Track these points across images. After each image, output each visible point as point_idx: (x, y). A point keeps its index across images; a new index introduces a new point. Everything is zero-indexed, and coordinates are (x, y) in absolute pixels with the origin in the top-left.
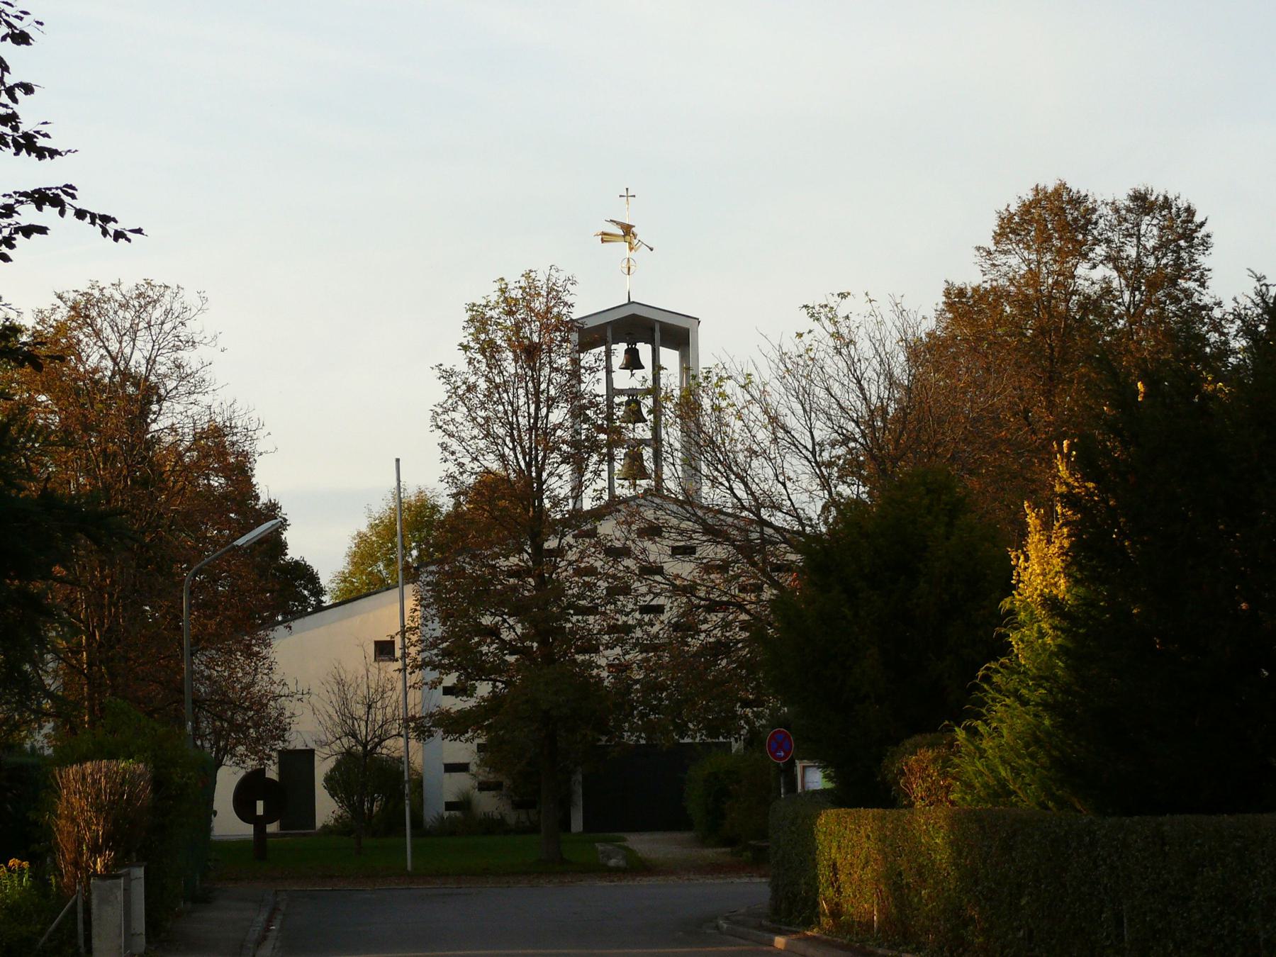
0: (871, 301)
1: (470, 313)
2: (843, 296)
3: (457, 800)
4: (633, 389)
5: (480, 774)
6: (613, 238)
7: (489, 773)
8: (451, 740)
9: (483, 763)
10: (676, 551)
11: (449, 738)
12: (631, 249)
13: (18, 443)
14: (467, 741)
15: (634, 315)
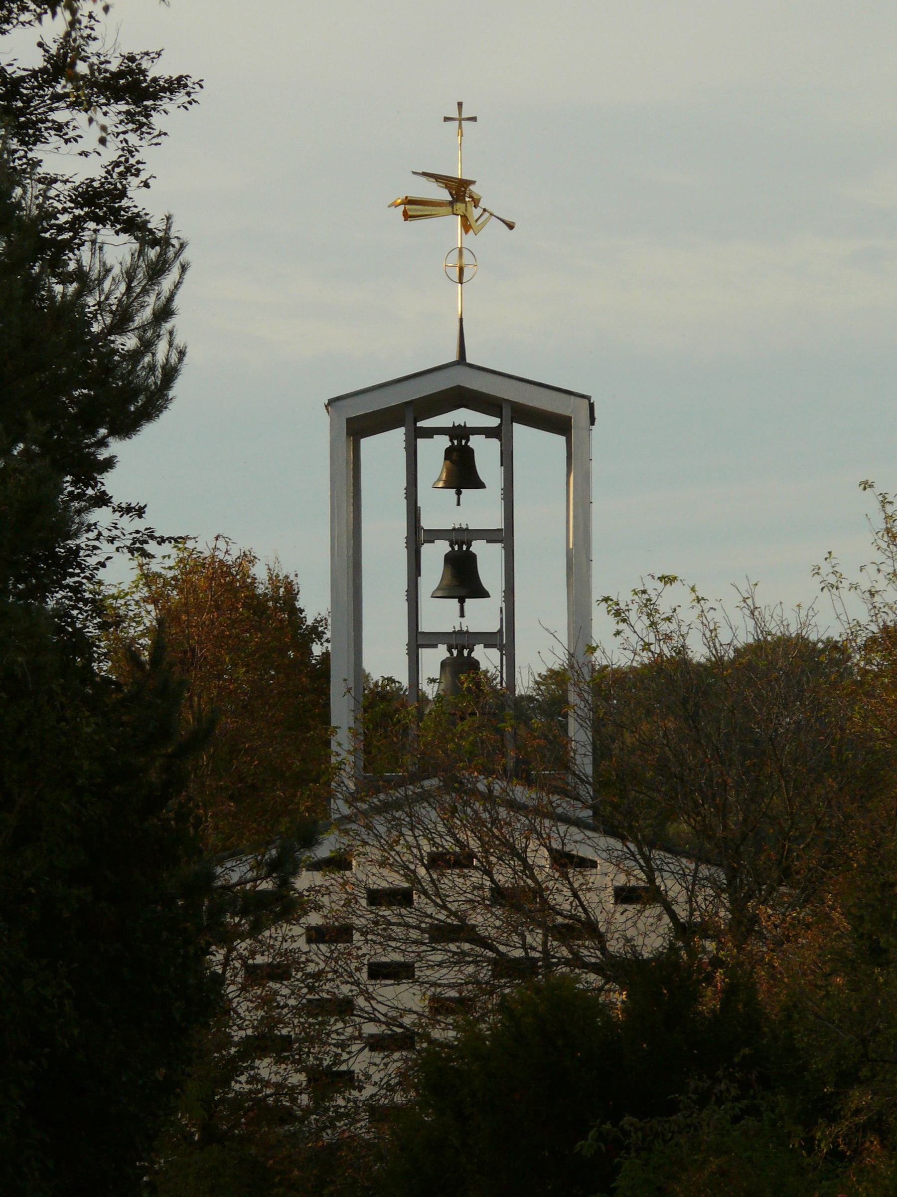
0: (699, 601)
2: (668, 580)
4: (460, 530)
12: (467, 226)
13: (537, 977)
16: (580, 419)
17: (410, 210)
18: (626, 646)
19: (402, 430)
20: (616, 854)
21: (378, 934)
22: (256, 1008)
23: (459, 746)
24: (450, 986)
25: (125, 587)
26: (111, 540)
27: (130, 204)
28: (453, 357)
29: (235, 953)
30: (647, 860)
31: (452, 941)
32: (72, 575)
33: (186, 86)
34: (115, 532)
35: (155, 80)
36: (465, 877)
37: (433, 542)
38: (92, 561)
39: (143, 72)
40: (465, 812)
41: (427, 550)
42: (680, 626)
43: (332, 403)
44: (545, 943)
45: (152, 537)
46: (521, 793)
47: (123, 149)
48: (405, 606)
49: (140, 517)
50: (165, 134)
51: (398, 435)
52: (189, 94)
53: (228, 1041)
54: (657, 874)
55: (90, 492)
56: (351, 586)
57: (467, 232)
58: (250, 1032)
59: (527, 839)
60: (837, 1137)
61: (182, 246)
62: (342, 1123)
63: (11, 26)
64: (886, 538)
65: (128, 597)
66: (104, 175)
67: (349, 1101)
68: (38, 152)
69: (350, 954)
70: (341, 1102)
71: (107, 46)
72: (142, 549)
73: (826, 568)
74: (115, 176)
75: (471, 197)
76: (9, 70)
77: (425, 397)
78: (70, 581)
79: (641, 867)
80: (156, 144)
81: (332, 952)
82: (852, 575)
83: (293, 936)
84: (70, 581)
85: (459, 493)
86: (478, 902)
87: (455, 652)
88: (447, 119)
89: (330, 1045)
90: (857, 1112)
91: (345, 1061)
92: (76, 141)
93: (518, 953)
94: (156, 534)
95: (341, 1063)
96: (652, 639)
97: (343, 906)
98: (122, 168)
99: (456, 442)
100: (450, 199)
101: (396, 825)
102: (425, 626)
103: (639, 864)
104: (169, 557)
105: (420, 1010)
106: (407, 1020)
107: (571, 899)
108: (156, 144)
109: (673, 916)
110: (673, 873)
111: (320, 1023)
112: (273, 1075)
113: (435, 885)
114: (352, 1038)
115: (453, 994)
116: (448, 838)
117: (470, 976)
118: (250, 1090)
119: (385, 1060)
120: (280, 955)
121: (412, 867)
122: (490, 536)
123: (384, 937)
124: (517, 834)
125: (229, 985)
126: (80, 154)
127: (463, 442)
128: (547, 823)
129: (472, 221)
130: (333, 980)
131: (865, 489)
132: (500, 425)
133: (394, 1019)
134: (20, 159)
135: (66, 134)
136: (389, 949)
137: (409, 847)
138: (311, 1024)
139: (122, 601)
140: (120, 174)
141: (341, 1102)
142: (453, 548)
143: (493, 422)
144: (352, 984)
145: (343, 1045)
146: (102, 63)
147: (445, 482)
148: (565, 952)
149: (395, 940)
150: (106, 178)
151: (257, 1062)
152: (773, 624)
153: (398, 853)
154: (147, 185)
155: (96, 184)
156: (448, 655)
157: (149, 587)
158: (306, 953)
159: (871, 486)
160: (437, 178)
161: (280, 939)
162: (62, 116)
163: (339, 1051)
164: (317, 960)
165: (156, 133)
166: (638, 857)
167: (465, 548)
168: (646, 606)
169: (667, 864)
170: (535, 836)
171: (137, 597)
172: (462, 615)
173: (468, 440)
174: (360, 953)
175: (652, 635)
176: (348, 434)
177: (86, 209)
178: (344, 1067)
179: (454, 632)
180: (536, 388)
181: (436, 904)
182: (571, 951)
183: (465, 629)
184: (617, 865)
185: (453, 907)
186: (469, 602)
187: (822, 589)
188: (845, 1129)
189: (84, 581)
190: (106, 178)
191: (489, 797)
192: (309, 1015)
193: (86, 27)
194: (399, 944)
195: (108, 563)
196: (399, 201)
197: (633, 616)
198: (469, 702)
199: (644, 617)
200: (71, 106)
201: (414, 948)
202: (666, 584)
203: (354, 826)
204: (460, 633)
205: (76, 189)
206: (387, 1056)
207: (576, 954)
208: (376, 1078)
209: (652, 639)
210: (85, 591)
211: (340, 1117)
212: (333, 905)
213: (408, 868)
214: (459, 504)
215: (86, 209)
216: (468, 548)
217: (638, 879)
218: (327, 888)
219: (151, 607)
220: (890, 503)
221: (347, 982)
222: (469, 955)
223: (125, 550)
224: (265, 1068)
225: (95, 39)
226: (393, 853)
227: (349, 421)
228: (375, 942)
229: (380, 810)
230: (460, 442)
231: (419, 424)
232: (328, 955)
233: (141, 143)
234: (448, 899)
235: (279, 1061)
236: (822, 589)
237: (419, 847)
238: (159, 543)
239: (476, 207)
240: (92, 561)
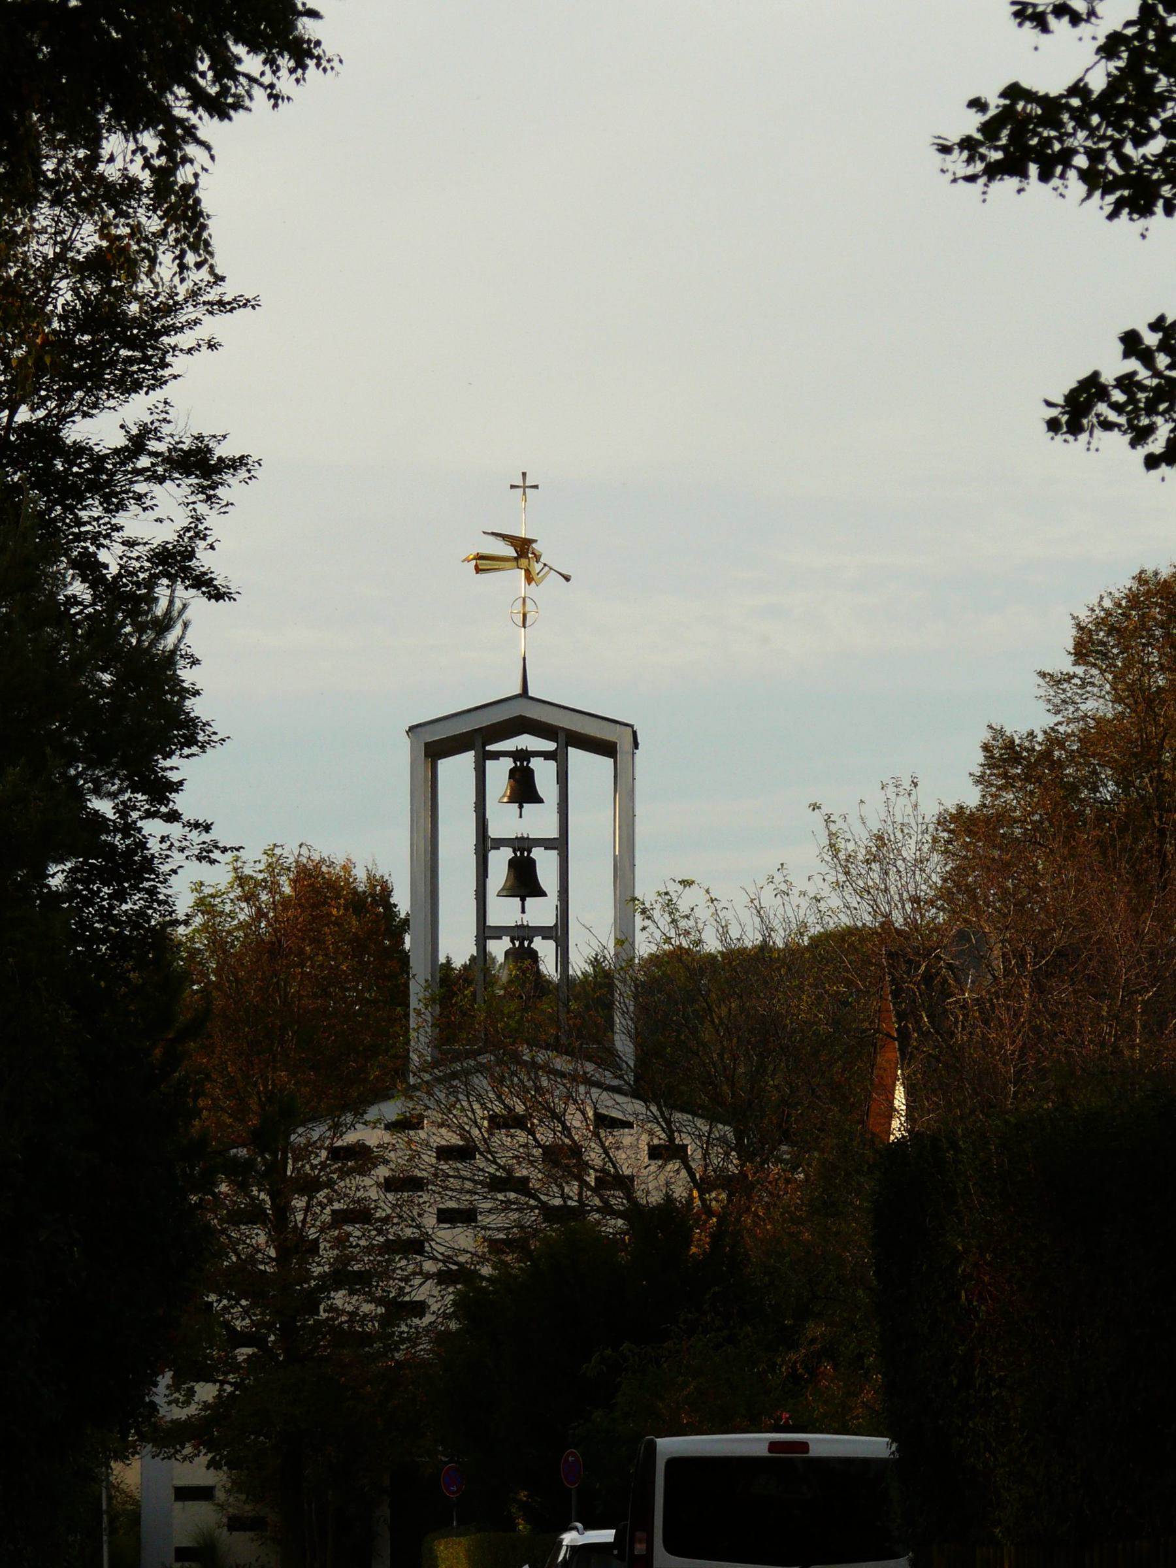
1: (195, 894)
2: (686, 883)
3: (189, 1545)
4: (522, 839)
5: (229, 1505)
6: (495, 564)
7: (245, 1502)
8: (163, 1459)
9: (237, 1486)
10: (446, 1217)
11: (161, 1456)
12: (529, 579)
14: (184, 1459)
15: (521, 716)
16: (624, 745)
17: (481, 564)
18: (651, 939)
19: (472, 753)
20: (641, 1117)
21: (437, 1185)
22: (331, 1248)
23: (507, 1024)
24: (499, 1230)
25: (222, 888)
26: (182, 850)
27: (198, 564)
28: (518, 690)
29: (315, 1200)
30: (668, 1122)
31: (500, 1191)
32: (148, 880)
33: (247, 464)
34: (185, 843)
35: (220, 459)
36: (512, 1136)
37: (498, 849)
38: (165, 868)
39: (209, 451)
40: (512, 1081)
41: (493, 856)
42: (697, 923)
43: (412, 729)
44: (580, 1194)
45: (217, 847)
46: (561, 1063)
47: (192, 517)
48: (473, 904)
49: (207, 832)
50: (232, 504)
51: (467, 759)
52: (249, 471)
53: (308, 1276)
54: (676, 1134)
55: (164, 809)
56: (428, 883)
57: (529, 584)
58: (326, 1268)
59: (566, 1104)
60: (796, 1362)
61: (185, 606)
62: (405, 1346)
63: (98, 411)
64: (830, 853)
65: (225, 896)
66: (176, 538)
67: (411, 1327)
68: (120, 519)
69: (412, 1201)
70: (404, 1328)
71: (179, 429)
72: (209, 857)
73: (778, 878)
74: (186, 540)
75: (533, 553)
76: (97, 449)
77: (491, 725)
78: (146, 885)
79: (663, 1129)
80: (225, 513)
81: (398, 1200)
82: (800, 884)
83: (364, 1187)
84: (146, 885)
85: (521, 807)
86: (523, 1158)
87: (517, 943)
88: (513, 487)
89: (394, 1279)
90: (813, 1341)
91: (408, 1293)
92: (153, 509)
93: (558, 1202)
94: (220, 845)
95: (405, 1295)
96: (672, 934)
97: (407, 1161)
98: (192, 533)
99: (518, 764)
100: (516, 555)
101: (453, 1091)
102: (492, 921)
103: (661, 1126)
104: (260, 861)
105: (473, 1250)
106: (462, 1259)
107: (603, 1156)
108: (225, 513)
109: (691, 1173)
110: (689, 1134)
111: (387, 1261)
112: (346, 1305)
113: (486, 1143)
114: (414, 1274)
115: (502, 1236)
116: (497, 1103)
117: (515, 1221)
118: (327, 1318)
119: (442, 1293)
120: (354, 1202)
121: (467, 1128)
122: (547, 844)
123: (442, 1187)
124: (556, 1100)
125: (309, 1228)
126: (156, 521)
127: (525, 763)
128: (582, 1089)
129: (534, 574)
130: (399, 1224)
131: (814, 809)
132: (556, 749)
133: (448, 1257)
134: (105, 524)
135: (144, 503)
136: (447, 1198)
137: (463, 1109)
138: (379, 1262)
139: (219, 900)
140: (190, 538)
141: (404, 1328)
142: (516, 854)
143: (550, 746)
144: (414, 1227)
145: (406, 1279)
146: (177, 443)
147: (509, 797)
148: (597, 1201)
149: (452, 1190)
150: (178, 541)
151: (332, 1294)
152: (777, 921)
153: (455, 1116)
154: (212, 547)
155: (170, 546)
156: (511, 946)
157: (242, 887)
158: (375, 1201)
159: (819, 808)
160: (504, 537)
161: (354, 1189)
162: (141, 488)
163: (403, 1285)
164: (385, 1207)
165: (224, 503)
166: (660, 1120)
167: (526, 854)
168: (668, 905)
169: (685, 1126)
170: (571, 1101)
171: (232, 896)
172: (523, 911)
173: (529, 762)
174: (421, 1200)
175: (673, 931)
176: (426, 756)
177: (161, 568)
178: (407, 1299)
179: (517, 926)
180: (587, 717)
181: (487, 1160)
182: (601, 1199)
183: (525, 923)
184: (642, 1127)
185: (501, 1162)
186: (530, 901)
187: (776, 895)
188: (802, 1355)
189: (159, 885)
190: (178, 541)
191: (533, 1066)
192: (380, 1254)
193: (162, 412)
194: (455, 1194)
195: (179, 871)
196: (472, 557)
197: (656, 914)
198: (517, 987)
199: (666, 915)
200: (148, 479)
201: (468, 1197)
202: (685, 887)
203: (418, 1094)
204: (521, 927)
205: (152, 550)
206: (444, 1289)
207: (605, 1202)
208: (434, 1308)
209: (672, 934)
210: (159, 893)
211: (403, 1341)
212: (399, 1160)
213: (464, 1129)
214: (521, 817)
215: (161, 568)
216: (529, 854)
217: (660, 1139)
218: (394, 1145)
219: (243, 905)
220: (834, 822)
221: (411, 1226)
222: (514, 1203)
223: (194, 858)
224: (339, 1298)
225: (169, 422)
226: (451, 1116)
227: (428, 745)
228: (434, 1192)
229: (438, 1080)
230: (522, 764)
231: (488, 748)
232: (394, 1202)
233: (210, 512)
234: (498, 1155)
235: (352, 1293)
236: (776, 895)
237: (473, 1111)
238: (223, 852)
239: (537, 562)
240: (165, 868)
